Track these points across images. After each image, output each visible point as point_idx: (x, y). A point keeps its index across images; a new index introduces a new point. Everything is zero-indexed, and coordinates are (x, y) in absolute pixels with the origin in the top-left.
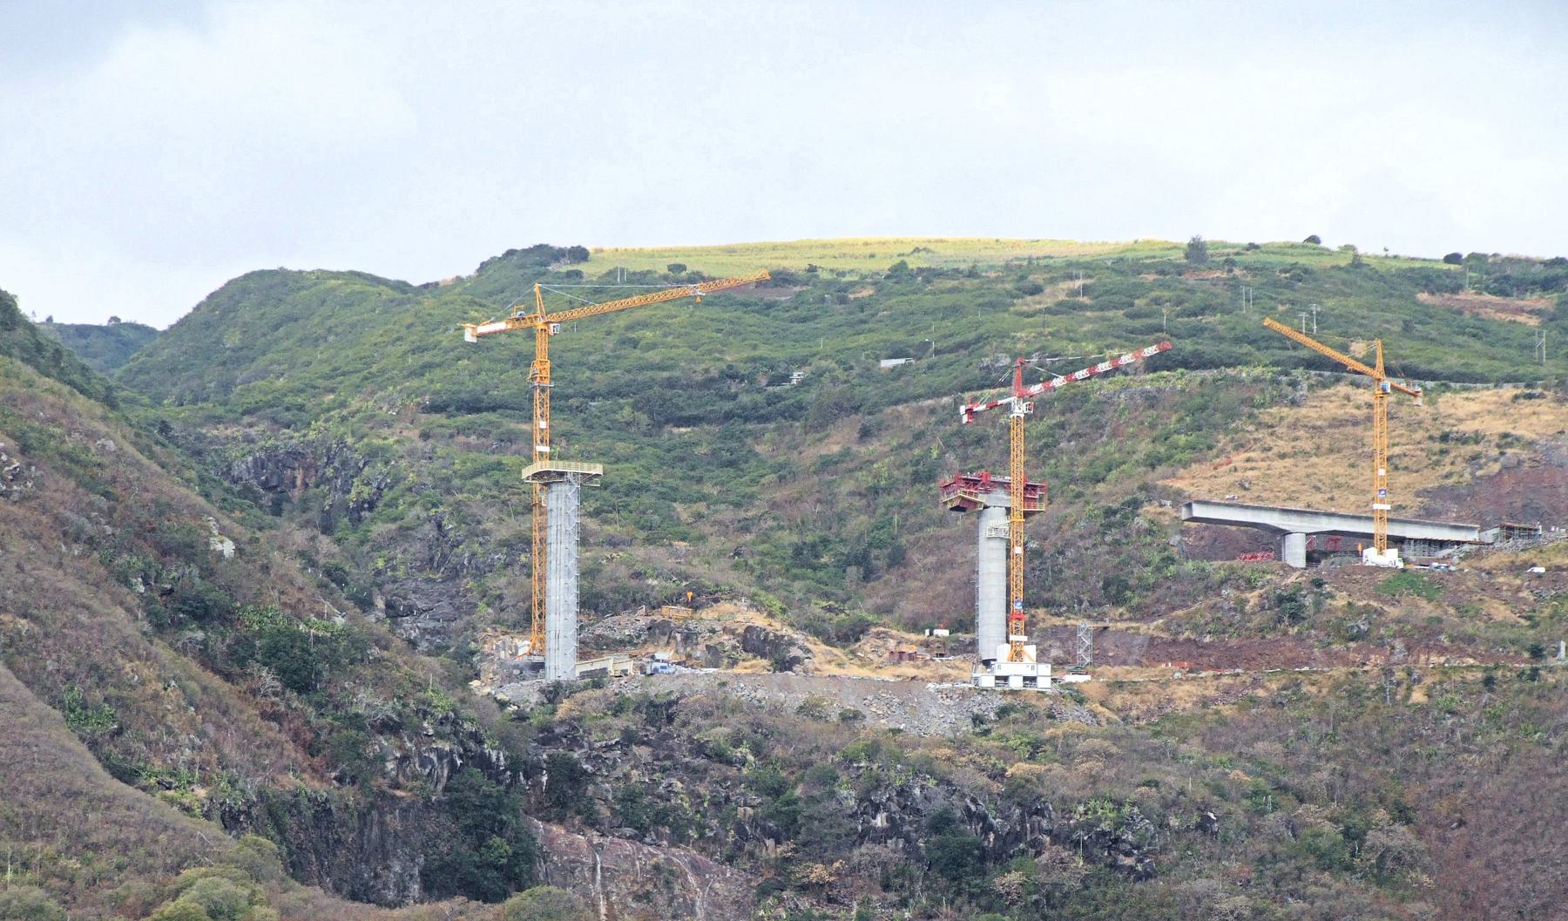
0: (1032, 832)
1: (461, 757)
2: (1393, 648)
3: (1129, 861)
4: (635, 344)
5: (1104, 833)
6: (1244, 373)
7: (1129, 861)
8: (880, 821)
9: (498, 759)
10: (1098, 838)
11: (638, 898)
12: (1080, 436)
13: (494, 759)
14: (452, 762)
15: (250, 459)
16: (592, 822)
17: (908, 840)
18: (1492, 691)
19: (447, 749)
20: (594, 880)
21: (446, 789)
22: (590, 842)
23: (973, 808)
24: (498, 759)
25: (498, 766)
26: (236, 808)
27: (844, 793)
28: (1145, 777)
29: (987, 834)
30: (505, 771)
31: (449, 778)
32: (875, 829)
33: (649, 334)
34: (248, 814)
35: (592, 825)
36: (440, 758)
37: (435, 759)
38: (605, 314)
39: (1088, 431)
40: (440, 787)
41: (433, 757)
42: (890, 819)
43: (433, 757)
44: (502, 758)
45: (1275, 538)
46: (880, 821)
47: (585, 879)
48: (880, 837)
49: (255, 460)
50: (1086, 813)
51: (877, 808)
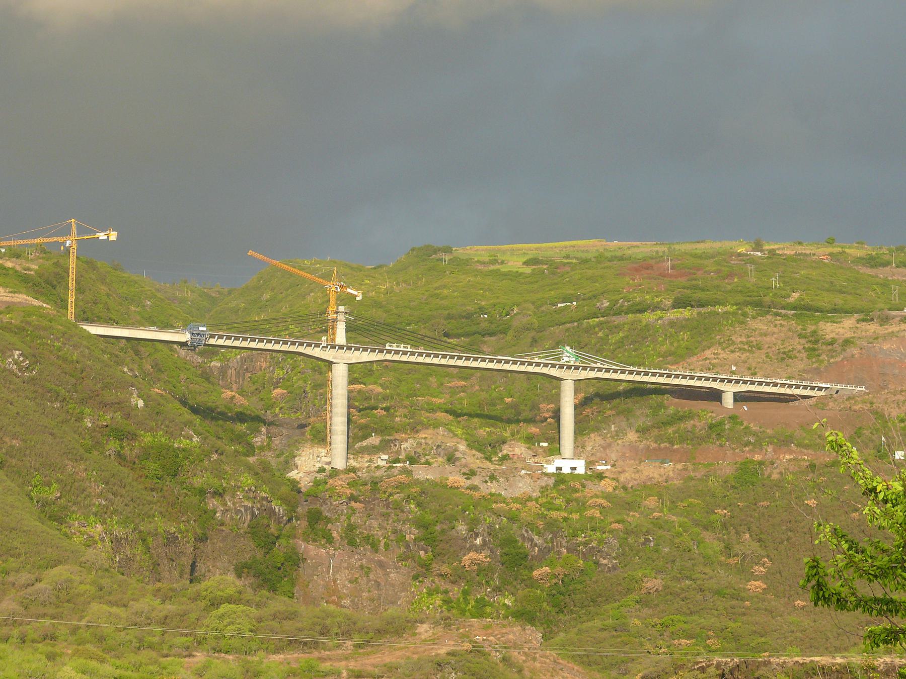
0: (557, 546)
1: (258, 509)
2: (767, 451)
3: (605, 562)
4: (437, 296)
5: (593, 548)
6: (720, 309)
7: (605, 562)
8: (478, 541)
9: (279, 510)
10: (590, 550)
11: (351, 582)
12: (636, 342)
13: (277, 510)
14: (253, 513)
15: (239, 357)
16: (330, 540)
17: (492, 551)
18: (813, 472)
19: (250, 505)
20: (328, 573)
21: (249, 526)
22: (328, 553)
23: (526, 535)
24: (279, 510)
25: (279, 515)
26: (119, 536)
27: (460, 528)
28: (619, 517)
29: (534, 548)
30: (283, 517)
31: (251, 520)
32: (476, 545)
33: (445, 291)
34: (126, 539)
35: (331, 543)
36: (246, 511)
37: (243, 511)
38: (807, 310)
39: (639, 340)
40: (246, 525)
41: (242, 509)
42: (484, 540)
43: (242, 509)
44: (281, 510)
45: (715, 396)
46: (478, 541)
47: (323, 572)
48: (478, 549)
49: (241, 358)
50: (585, 537)
51: (477, 535)
